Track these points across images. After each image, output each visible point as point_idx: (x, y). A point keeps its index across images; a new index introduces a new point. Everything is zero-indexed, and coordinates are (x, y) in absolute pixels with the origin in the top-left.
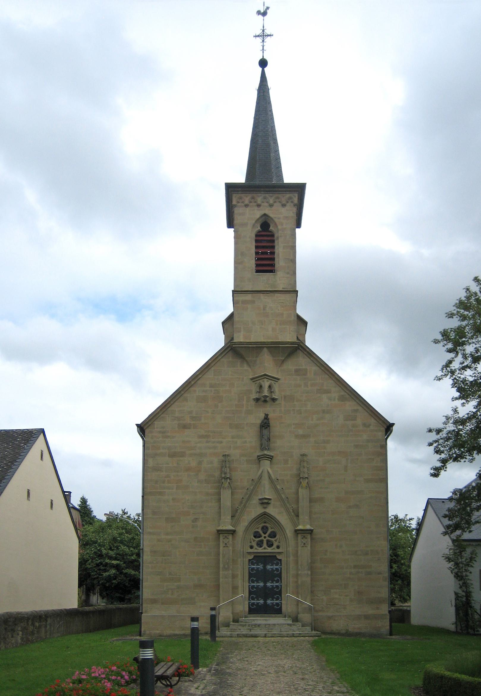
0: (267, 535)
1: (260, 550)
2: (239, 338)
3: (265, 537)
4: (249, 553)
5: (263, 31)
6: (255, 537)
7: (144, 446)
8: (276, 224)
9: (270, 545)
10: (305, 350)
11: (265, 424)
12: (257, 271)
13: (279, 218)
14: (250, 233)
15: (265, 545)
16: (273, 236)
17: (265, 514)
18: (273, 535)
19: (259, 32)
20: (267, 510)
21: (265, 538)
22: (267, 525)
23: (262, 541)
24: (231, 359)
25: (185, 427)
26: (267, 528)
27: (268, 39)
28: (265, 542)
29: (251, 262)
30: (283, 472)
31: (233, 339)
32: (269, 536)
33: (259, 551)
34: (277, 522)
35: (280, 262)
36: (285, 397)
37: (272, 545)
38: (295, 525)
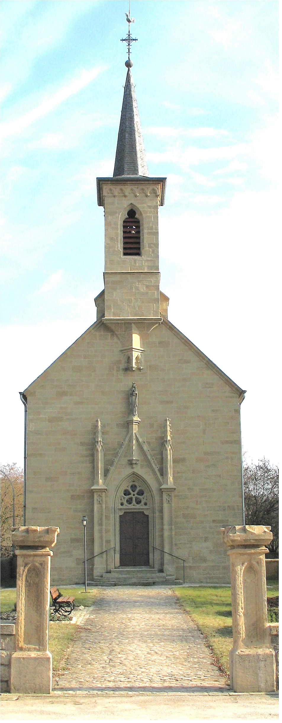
0: (135, 493)
1: (130, 506)
2: (108, 316)
3: (134, 495)
4: (121, 509)
5: (129, 35)
6: (125, 494)
7: (26, 411)
8: (141, 213)
9: (138, 502)
10: (168, 325)
11: (131, 394)
12: (125, 254)
13: (144, 208)
14: (121, 216)
15: (134, 502)
16: (139, 222)
17: (134, 473)
18: (141, 493)
19: (125, 37)
20: (135, 470)
21: (134, 495)
22: (137, 484)
23: (131, 499)
24: (102, 333)
25: (64, 394)
26: (135, 486)
27: (133, 43)
28: (134, 499)
29: (120, 246)
30: (100, 449)
31: (103, 316)
32: (138, 494)
33: (130, 507)
34: (144, 481)
35: (145, 247)
36: (150, 366)
37: (140, 502)
38: (160, 484)
